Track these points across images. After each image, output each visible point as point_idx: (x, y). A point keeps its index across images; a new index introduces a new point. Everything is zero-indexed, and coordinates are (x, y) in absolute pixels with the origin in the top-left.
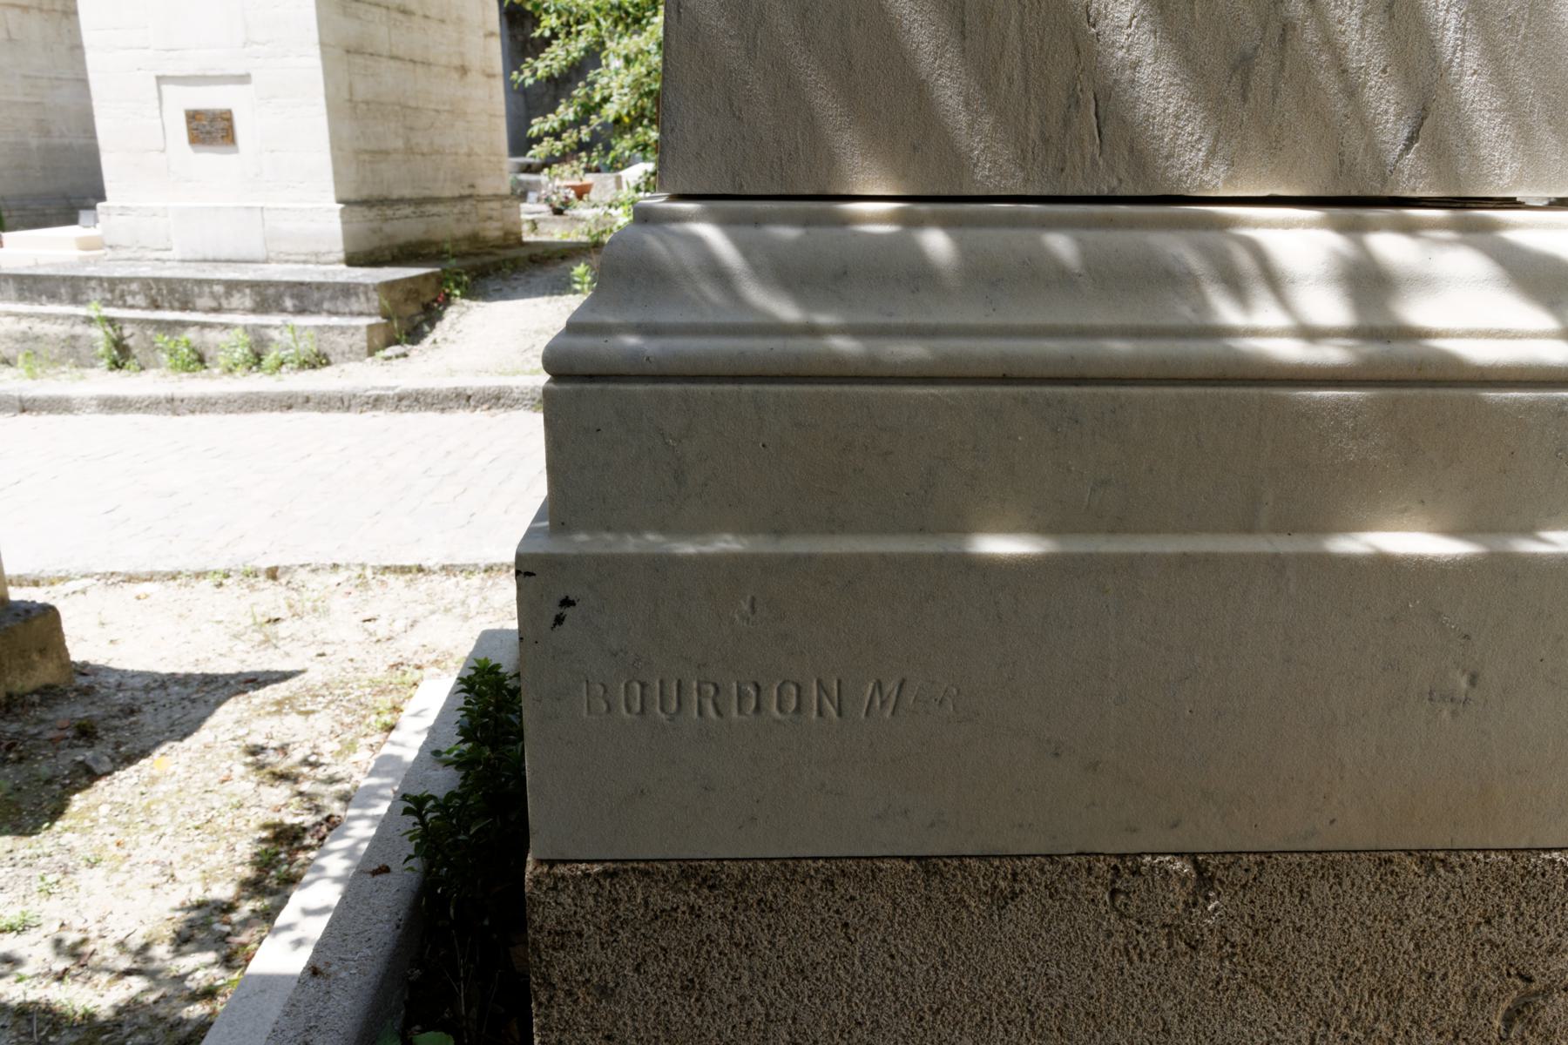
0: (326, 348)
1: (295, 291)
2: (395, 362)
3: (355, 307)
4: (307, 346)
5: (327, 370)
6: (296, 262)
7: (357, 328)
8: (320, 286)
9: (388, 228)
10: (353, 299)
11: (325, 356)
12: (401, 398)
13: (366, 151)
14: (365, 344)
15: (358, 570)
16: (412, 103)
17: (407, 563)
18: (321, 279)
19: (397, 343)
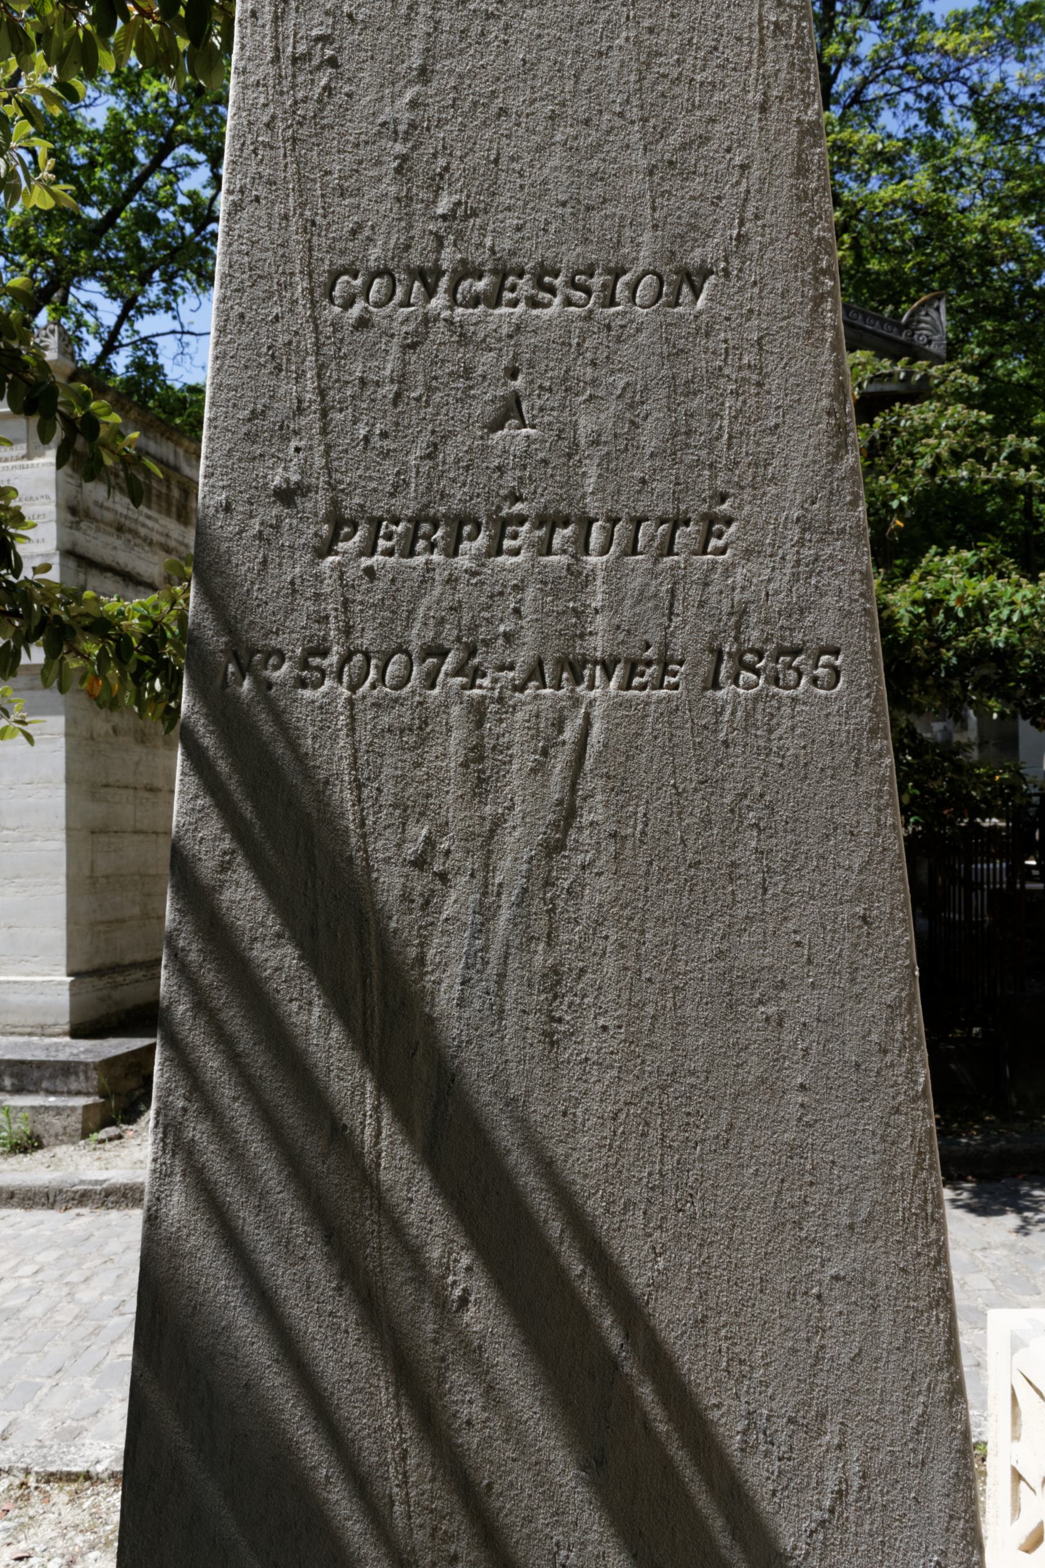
0: (39, 1129)
1: (16, 1070)
2: (108, 1145)
3: (74, 1086)
4: (21, 1127)
5: (38, 1155)
6: (21, 1034)
7: (73, 1109)
8: (40, 1065)
9: (117, 995)
10: (73, 1078)
11: (38, 1138)
12: (108, 1193)
13: (102, 922)
14: (79, 1126)
15: (22, 1477)
16: (152, 871)
17: (74, 1469)
18: (41, 1056)
19: (112, 1123)
